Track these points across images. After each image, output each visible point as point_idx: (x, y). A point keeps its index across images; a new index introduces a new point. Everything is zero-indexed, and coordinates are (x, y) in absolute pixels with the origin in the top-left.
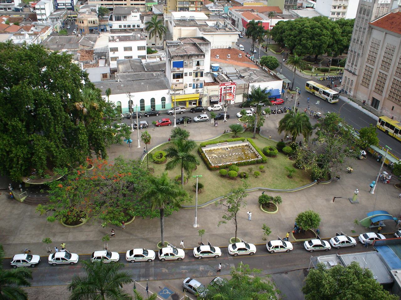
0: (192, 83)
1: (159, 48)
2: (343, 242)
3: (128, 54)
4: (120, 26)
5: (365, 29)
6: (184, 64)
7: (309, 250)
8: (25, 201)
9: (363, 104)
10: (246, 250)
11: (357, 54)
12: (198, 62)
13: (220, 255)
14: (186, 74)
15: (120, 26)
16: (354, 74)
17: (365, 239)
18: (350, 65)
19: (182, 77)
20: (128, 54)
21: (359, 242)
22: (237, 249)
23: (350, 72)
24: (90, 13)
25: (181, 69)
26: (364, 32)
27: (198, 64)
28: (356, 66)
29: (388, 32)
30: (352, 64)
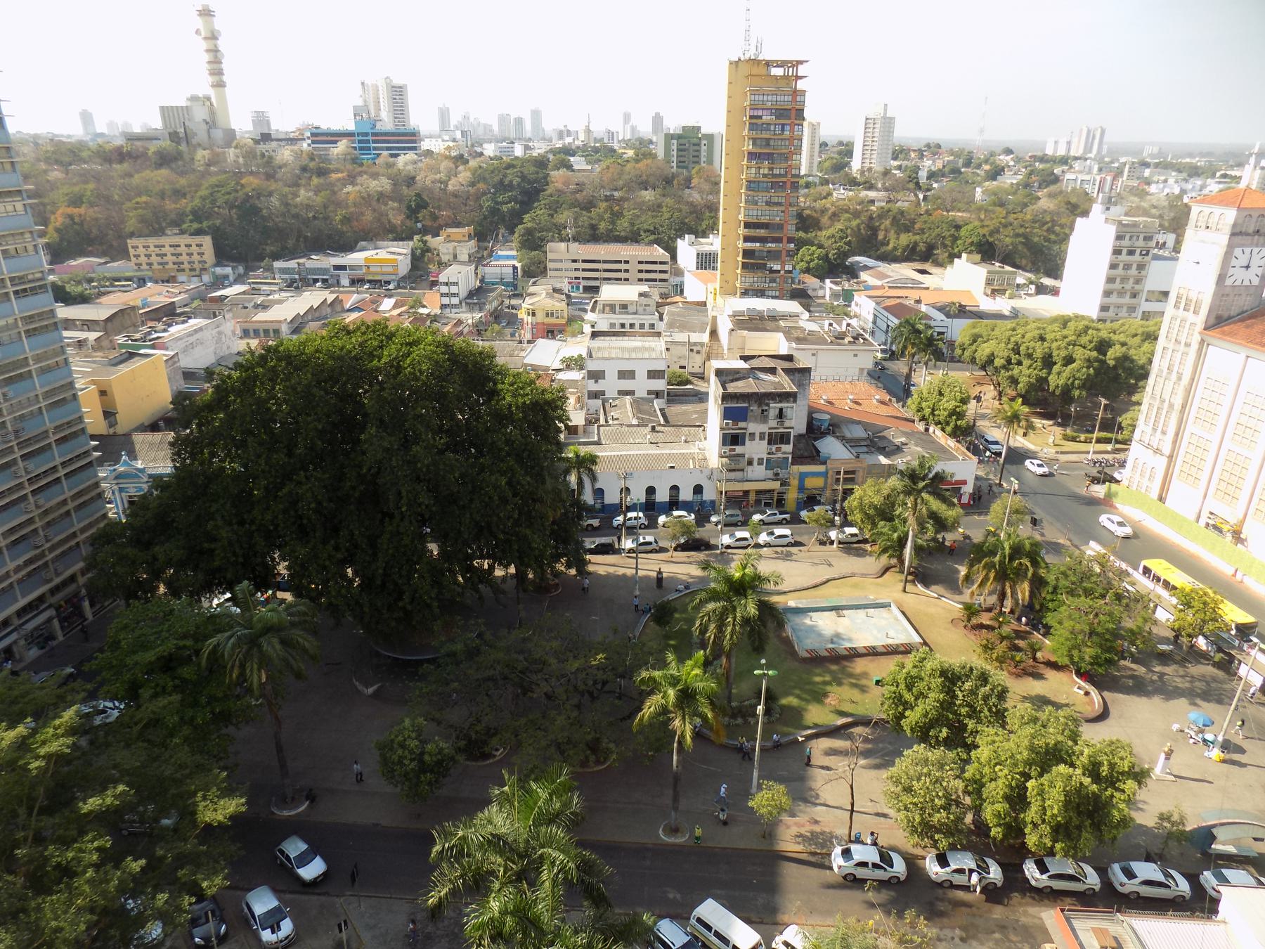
0: (765, 456)
1: (693, 374)
2: (863, 864)
3: (626, 385)
4: (613, 325)
5: (1188, 345)
6: (750, 414)
7: (1041, 886)
8: (376, 695)
9: (866, 268)
10: (1077, 880)
11: (1166, 405)
12: (781, 410)
13: (1097, 888)
14: (752, 435)
15: (613, 325)
16: (1157, 451)
17: (1037, 875)
18: (1149, 430)
19: (743, 444)
20: (626, 385)
21: (1107, 884)
22: (852, 863)
23: (1149, 446)
24: (549, 295)
25: (741, 424)
26: (1185, 354)
27: (781, 414)
28: (1164, 433)
29: (1251, 353)
30: (1155, 430)
